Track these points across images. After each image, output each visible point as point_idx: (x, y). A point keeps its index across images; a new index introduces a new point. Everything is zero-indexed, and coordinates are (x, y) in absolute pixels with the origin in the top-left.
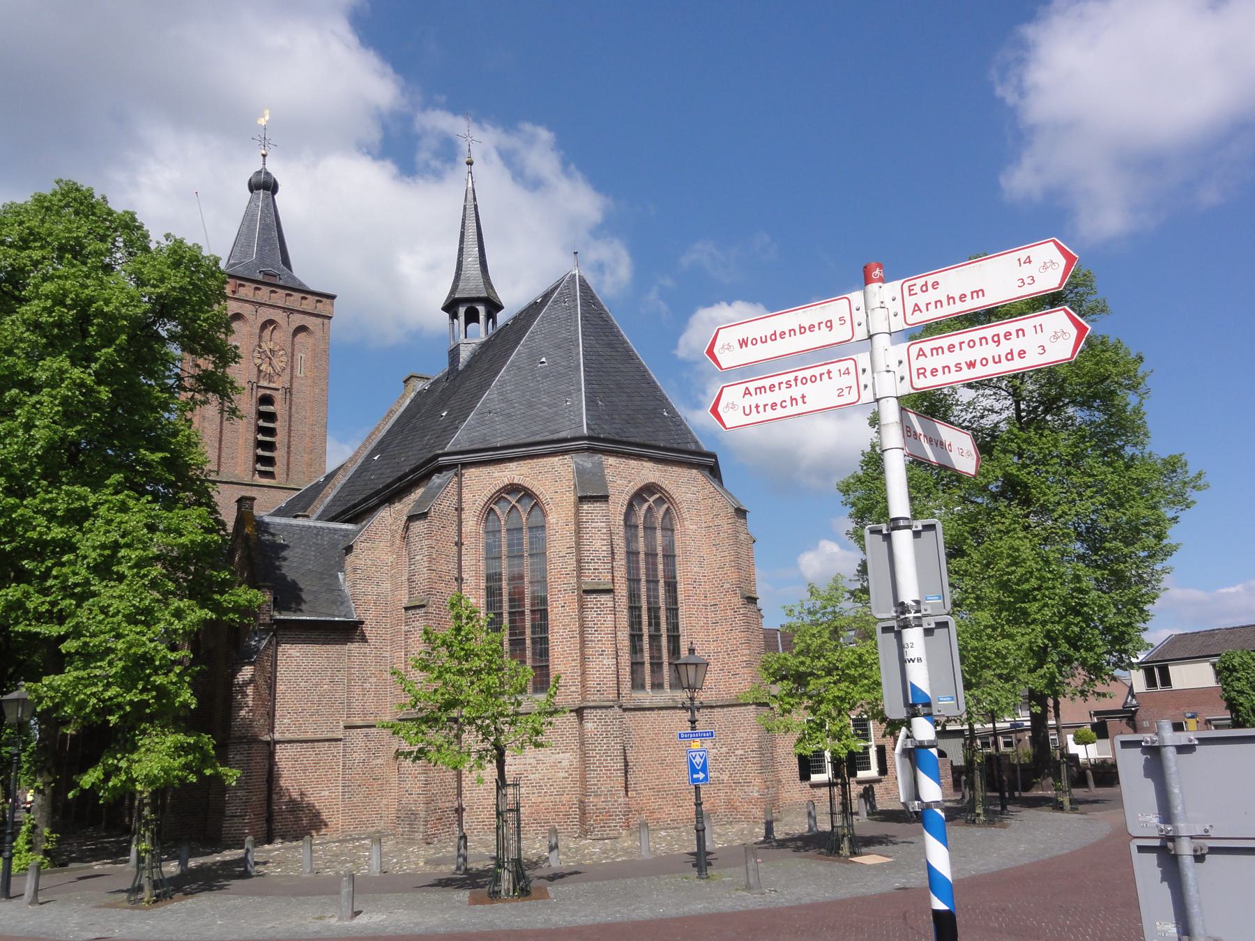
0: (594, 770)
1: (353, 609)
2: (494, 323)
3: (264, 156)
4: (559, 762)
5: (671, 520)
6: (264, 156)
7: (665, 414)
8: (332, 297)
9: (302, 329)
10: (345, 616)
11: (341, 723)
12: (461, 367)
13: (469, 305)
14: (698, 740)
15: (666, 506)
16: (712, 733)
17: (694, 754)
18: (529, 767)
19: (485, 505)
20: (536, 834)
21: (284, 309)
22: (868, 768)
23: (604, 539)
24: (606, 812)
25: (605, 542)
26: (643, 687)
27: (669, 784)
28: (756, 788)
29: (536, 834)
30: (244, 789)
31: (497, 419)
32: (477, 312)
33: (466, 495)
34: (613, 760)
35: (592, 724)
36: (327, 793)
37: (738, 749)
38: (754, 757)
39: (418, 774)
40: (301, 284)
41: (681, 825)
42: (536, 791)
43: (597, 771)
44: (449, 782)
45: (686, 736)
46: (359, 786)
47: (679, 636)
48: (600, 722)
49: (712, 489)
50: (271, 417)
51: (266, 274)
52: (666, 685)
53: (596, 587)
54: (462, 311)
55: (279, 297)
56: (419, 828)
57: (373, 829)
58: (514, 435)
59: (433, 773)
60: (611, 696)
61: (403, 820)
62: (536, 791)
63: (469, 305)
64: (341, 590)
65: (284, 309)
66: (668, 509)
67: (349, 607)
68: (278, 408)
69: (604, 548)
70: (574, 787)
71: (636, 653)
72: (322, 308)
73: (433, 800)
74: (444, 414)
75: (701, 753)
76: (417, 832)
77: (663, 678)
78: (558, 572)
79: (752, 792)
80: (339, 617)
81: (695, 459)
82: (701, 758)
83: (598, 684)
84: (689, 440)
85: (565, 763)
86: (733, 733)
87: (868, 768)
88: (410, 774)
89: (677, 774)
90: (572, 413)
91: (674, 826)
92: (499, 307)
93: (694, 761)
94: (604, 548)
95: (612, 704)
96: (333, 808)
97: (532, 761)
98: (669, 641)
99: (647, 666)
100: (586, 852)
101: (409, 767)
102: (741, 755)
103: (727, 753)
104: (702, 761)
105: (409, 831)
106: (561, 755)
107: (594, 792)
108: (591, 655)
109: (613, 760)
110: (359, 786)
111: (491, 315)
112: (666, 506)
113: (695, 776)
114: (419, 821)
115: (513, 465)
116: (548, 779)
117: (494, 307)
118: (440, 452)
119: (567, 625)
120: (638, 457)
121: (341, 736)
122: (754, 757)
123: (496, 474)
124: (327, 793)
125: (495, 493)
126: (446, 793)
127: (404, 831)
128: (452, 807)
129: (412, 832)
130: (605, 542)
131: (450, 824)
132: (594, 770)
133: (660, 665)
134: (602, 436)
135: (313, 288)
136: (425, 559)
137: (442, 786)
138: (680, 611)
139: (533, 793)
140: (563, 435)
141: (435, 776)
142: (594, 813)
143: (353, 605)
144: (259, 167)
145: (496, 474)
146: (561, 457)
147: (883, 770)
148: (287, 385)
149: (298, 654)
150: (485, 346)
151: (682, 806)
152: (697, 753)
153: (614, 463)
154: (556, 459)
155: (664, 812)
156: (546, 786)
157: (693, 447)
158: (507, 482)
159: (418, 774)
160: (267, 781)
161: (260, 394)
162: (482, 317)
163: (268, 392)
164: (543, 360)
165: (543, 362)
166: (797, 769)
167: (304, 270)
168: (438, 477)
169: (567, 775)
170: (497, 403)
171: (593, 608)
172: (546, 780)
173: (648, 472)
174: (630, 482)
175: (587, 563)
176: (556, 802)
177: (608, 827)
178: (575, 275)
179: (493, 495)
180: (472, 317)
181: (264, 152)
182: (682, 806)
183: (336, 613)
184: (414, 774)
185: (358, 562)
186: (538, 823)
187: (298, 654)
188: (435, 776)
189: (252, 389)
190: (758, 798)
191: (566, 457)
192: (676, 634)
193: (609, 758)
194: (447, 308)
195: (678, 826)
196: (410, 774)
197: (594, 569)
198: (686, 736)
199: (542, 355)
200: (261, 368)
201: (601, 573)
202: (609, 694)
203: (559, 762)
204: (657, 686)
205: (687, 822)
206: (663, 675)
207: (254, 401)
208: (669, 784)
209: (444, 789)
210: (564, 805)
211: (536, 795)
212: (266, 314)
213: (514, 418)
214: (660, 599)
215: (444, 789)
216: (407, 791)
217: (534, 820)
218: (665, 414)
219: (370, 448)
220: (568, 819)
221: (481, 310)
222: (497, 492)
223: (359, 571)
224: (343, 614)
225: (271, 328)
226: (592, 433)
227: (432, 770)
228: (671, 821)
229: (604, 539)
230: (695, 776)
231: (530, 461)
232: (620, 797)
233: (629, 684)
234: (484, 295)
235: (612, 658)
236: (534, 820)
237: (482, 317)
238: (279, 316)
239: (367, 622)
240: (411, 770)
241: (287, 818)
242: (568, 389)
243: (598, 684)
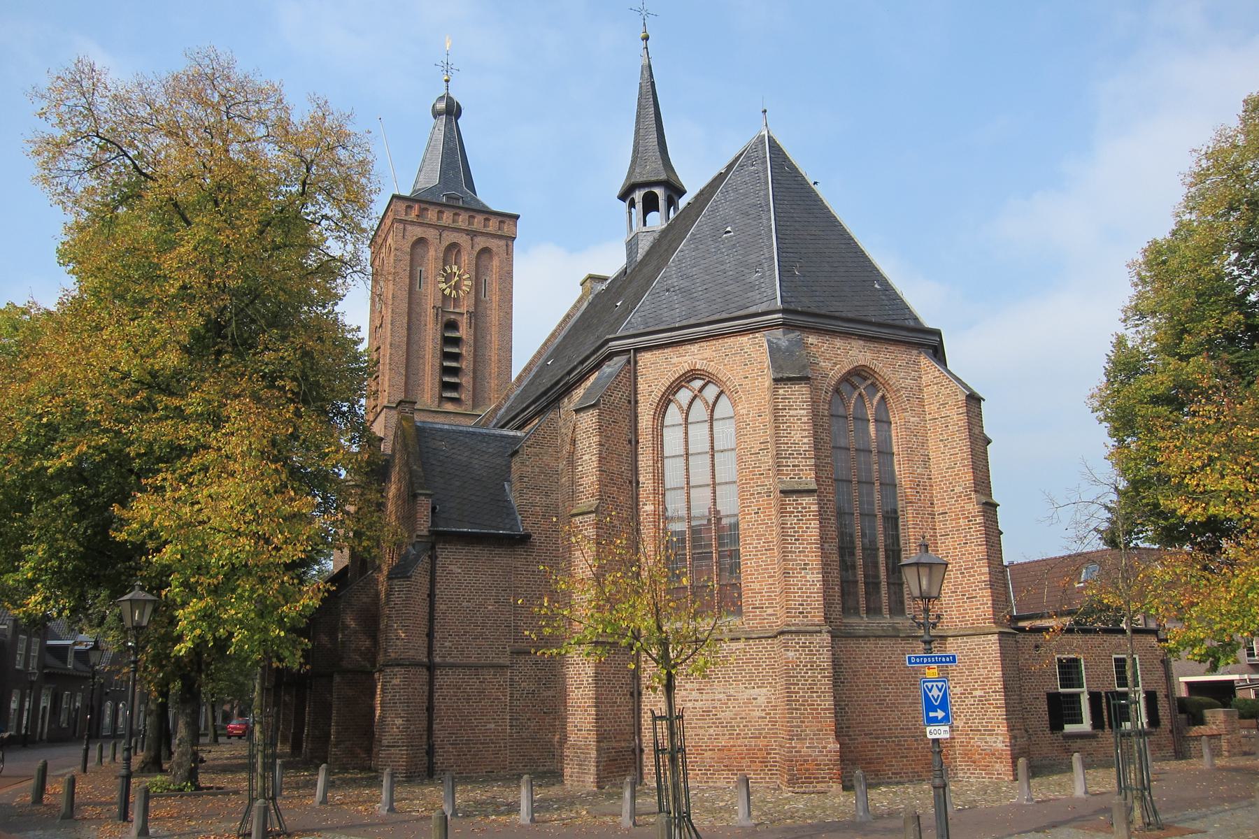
0: (797, 709)
1: (519, 522)
2: (676, 209)
3: (447, 81)
4: (754, 699)
5: (887, 411)
6: (447, 81)
7: (877, 286)
8: (517, 217)
9: (486, 251)
10: (510, 529)
11: (508, 649)
12: (639, 257)
13: (647, 190)
14: (935, 666)
15: (880, 394)
16: (954, 657)
17: (930, 685)
18: (717, 704)
19: (662, 396)
20: (728, 782)
21: (467, 232)
22: (1079, 720)
23: (805, 430)
24: (813, 761)
25: (806, 433)
26: (857, 612)
27: (891, 729)
28: (1001, 738)
29: (728, 782)
30: (401, 717)
31: (675, 297)
32: (655, 196)
33: (642, 386)
34: (820, 697)
35: (793, 654)
36: (493, 726)
37: (977, 689)
38: (997, 700)
39: (588, 707)
40: (484, 206)
41: (906, 779)
42: (727, 733)
43: (800, 709)
44: (624, 718)
45: (918, 660)
46: (529, 719)
47: (900, 551)
48: (804, 651)
49: (937, 374)
50: (456, 342)
51: (449, 197)
52: (885, 610)
53: (796, 487)
54: (638, 195)
55: (462, 220)
56: (589, 770)
57: (545, 769)
58: (695, 313)
59: (605, 707)
60: (816, 619)
61: (572, 760)
62: (727, 733)
63: (647, 190)
64: (507, 501)
65: (467, 232)
66: (883, 397)
67: (515, 519)
68: (464, 332)
69: (806, 440)
70: (773, 729)
71: (847, 570)
72: (506, 229)
73: (605, 738)
74: (618, 304)
75: (940, 684)
76: (586, 773)
77: (880, 601)
78: (750, 472)
79: (995, 742)
80: (503, 530)
81: (915, 338)
82: (940, 691)
83: (799, 605)
84: (907, 316)
85: (762, 700)
86: (970, 669)
87: (1079, 720)
88: (580, 707)
89: (899, 718)
90: (763, 285)
91: (896, 780)
92: (681, 192)
93: (930, 695)
94: (806, 440)
95: (818, 628)
96: (500, 743)
97: (721, 696)
98: (887, 557)
99: (862, 587)
100: (786, 807)
101: (578, 699)
102: (980, 696)
103: (961, 694)
104: (941, 694)
105: (578, 773)
106: (756, 690)
107: (797, 735)
108: (792, 569)
109: (820, 697)
110: (529, 719)
111: (671, 202)
112: (880, 394)
113: (932, 714)
114: (590, 762)
115: (694, 348)
116: (742, 718)
117: (675, 191)
118: (610, 337)
119: (762, 535)
120: (846, 335)
121: (508, 663)
122: (997, 700)
123: (675, 360)
124: (493, 726)
125: (674, 382)
126: (620, 730)
127: (572, 772)
128: (628, 747)
129: (582, 773)
130: (806, 433)
131: (627, 767)
132: (797, 709)
133: (877, 585)
134: (800, 309)
135: (495, 208)
136: (594, 459)
137: (616, 722)
138: (900, 520)
139: (724, 735)
140: (753, 310)
141: (608, 710)
142: (797, 761)
143: (520, 517)
144: (443, 92)
145: (675, 360)
146: (751, 336)
147: (1154, 720)
148: (472, 309)
149: (460, 571)
150: (664, 233)
151: (907, 757)
152: (935, 684)
153: (815, 342)
154: (745, 339)
155: (885, 763)
156: (738, 726)
157: (912, 323)
158: (687, 368)
159: (588, 707)
160: (428, 709)
161: (445, 319)
162: (662, 203)
163: (453, 317)
164: (729, 229)
165: (729, 232)
166: (1047, 717)
167: (489, 194)
168: (608, 366)
169: (763, 715)
170: (675, 280)
171: (793, 512)
172: (738, 719)
173: (856, 354)
174: (835, 364)
175: (785, 458)
176: (750, 746)
177: (814, 778)
178: (764, 135)
179: (672, 384)
180: (650, 204)
181: (446, 78)
182: (907, 757)
183: (501, 525)
184: (584, 707)
185: (525, 469)
186: (729, 770)
187: (460, 571)
188: (608, 710)
189: (437, 314)
190: (1002, 750)
191: (757, 335)
192: (896, 548)
193: (815, 695)
194: (623, 197)
195: (902, 780)
196: (580, 707)
197: (793, 466)
198: (918, 660)
199: (727, 224)
200: (445, 292)
201: (802, 470)
202: (814, 616)
203: (754, 699)
204: (874, 610)
205: (914, 777)
206: (880, 597)
207: (439, 326)
208: (891, 729)
209: (619, 726)
210: (761, 750)
211: (728, 737)
212: (450, 237)
213: (695, 295)
214: (876, 505)
215: (619, 726)
216: (576, 726)
217: (724, 766)
218: (877, 286)
219: (545, 356)
220: (766, 766)
221: (660, 192)
222: (676, 380)
223: (526, 479)
224: (508, 526)
225: (454, 253)
226: (786, 306)
227: (604, 703)
228: (892, 774)
229: (805, 430)
230: (932, 714)
231: (714, 342)
232: (830, 743)
233: (839, 608)
234: (663, 177)
235: (818, 573)
236: (724, 766)
237: (662, 203)
238: (463, 240)
239: (535, 536)
240: (580, 703)
241: (449, 752)
242: (758, 259)
243: (799, 605)
